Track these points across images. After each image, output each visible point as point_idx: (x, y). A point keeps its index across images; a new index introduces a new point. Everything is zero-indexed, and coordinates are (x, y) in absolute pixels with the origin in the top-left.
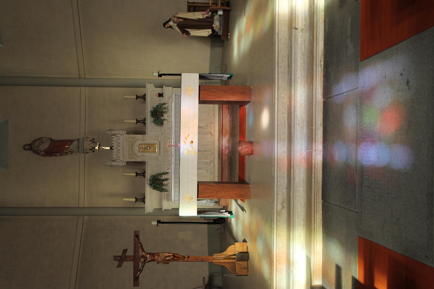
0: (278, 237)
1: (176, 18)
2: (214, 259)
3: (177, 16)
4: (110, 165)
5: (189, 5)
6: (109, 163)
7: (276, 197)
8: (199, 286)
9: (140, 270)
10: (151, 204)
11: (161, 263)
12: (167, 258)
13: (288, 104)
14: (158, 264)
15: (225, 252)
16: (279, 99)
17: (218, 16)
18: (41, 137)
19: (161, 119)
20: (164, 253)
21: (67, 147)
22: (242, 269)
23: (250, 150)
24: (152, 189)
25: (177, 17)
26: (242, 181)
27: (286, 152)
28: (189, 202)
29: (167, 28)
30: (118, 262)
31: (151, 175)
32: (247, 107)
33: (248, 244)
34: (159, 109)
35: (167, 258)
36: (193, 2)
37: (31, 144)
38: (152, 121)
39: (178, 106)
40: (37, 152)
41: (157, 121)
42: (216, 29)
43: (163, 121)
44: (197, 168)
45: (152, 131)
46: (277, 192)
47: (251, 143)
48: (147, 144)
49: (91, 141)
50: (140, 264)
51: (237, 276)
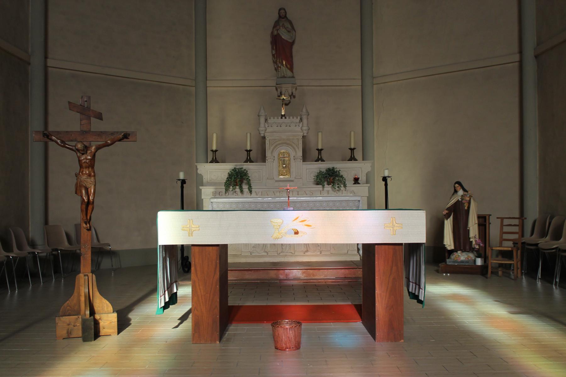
1: (468, 199)
5: (487, 217)
6: (263, 113)
9: (62, 142)
10: (208, 171)
11: (77, 179)
12: (84, 192)
14: (76, 174)
17: (474, 258)
18: (296, 30)
19: (324, 182)
20: (95, 185)
23: (284, 345)
24: (229, 171)
25: (470, 200)
29: (454, 186)
31: (248, 171)
32: (359, 325)
34: (338, 179)
36: (490, 222)
37: (287, 18)
38: (321, 170)
40: (276, 24)
42: (454, 256)
43: (321, 185)
47: (298, 347)
48: (289, 164)
49: (292, 93)
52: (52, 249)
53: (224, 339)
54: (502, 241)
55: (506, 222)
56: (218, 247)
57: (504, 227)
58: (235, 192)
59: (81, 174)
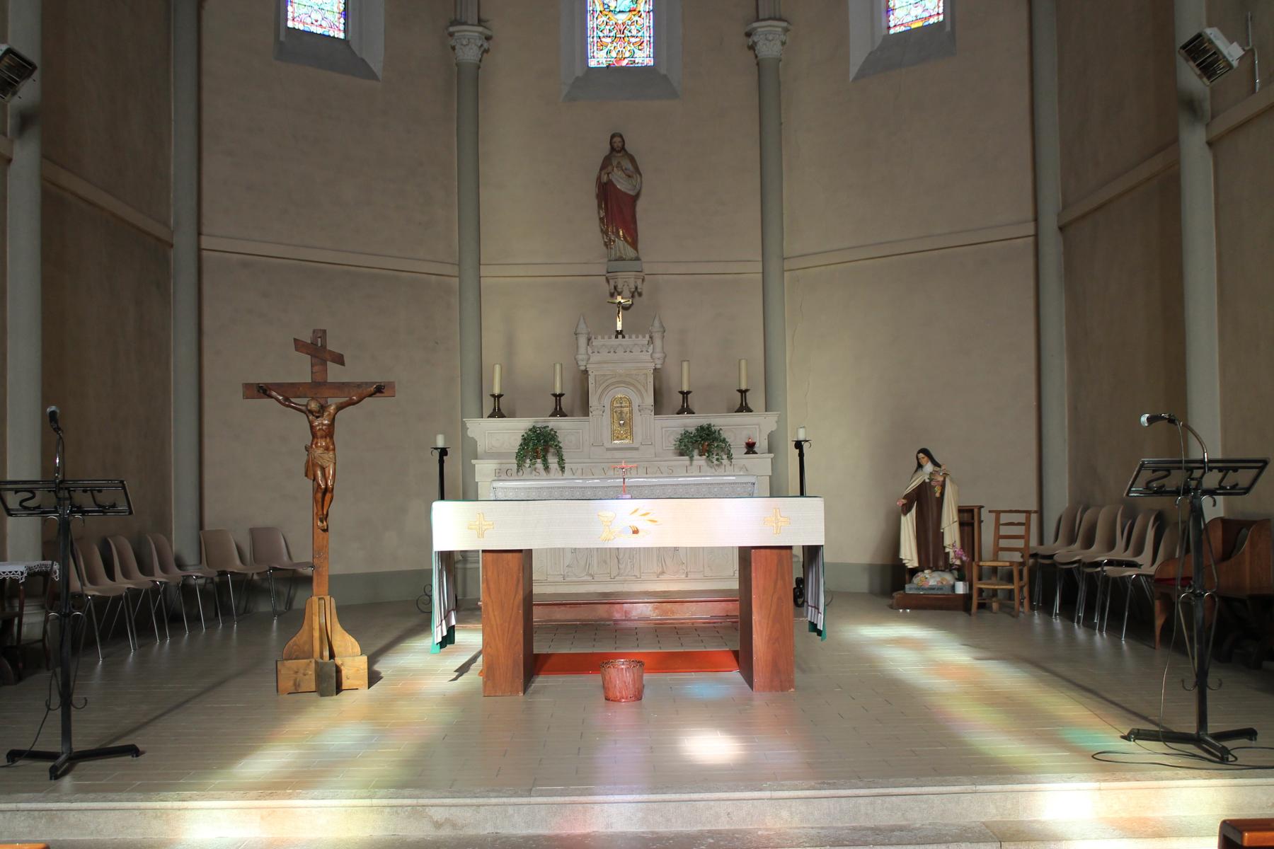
0: (346, 811)
1: (941, 479)
2: (319, 599)
5: (976, 511)
6: (582, 328)
7: (468, 801)
8: (292, 554)
9: (287, 399)
10: (487, 432)
12: (319, 473)
13: (760, 833)
14: (306, 447)
15: (341, 629)
16: (773, 801)
17: (952, 583)
18: (642, 172)
19: (692, 451)
20: (335, 464)
21: (619, 232)
22: (295, 676)
23: (618, 694)
24: (523, 432)
25: (944, 481)
26: (534, 665)
27: (610, 830)
28: (471, 529)
30: (310, 342)
32: (736, 675)
33: (364, 692)
34: (717, 446)
35: (319, 473)
37: (625, 151)
38: (687, 429)
41: (688, 442)
42: (918, 579)
44: (563, 549)
46: (483, 805)
47: (638, 696)
48: (631, 419)
49: (636, 288)
50: (303, 401)
51: (277, 662)
52: (218, 572)
53: (530, 690)
54: (998, 552)
55: (1004, 518)
56: (521, 554)
57: (1001, 527)
58: (535, 469)
59: (314, 446)
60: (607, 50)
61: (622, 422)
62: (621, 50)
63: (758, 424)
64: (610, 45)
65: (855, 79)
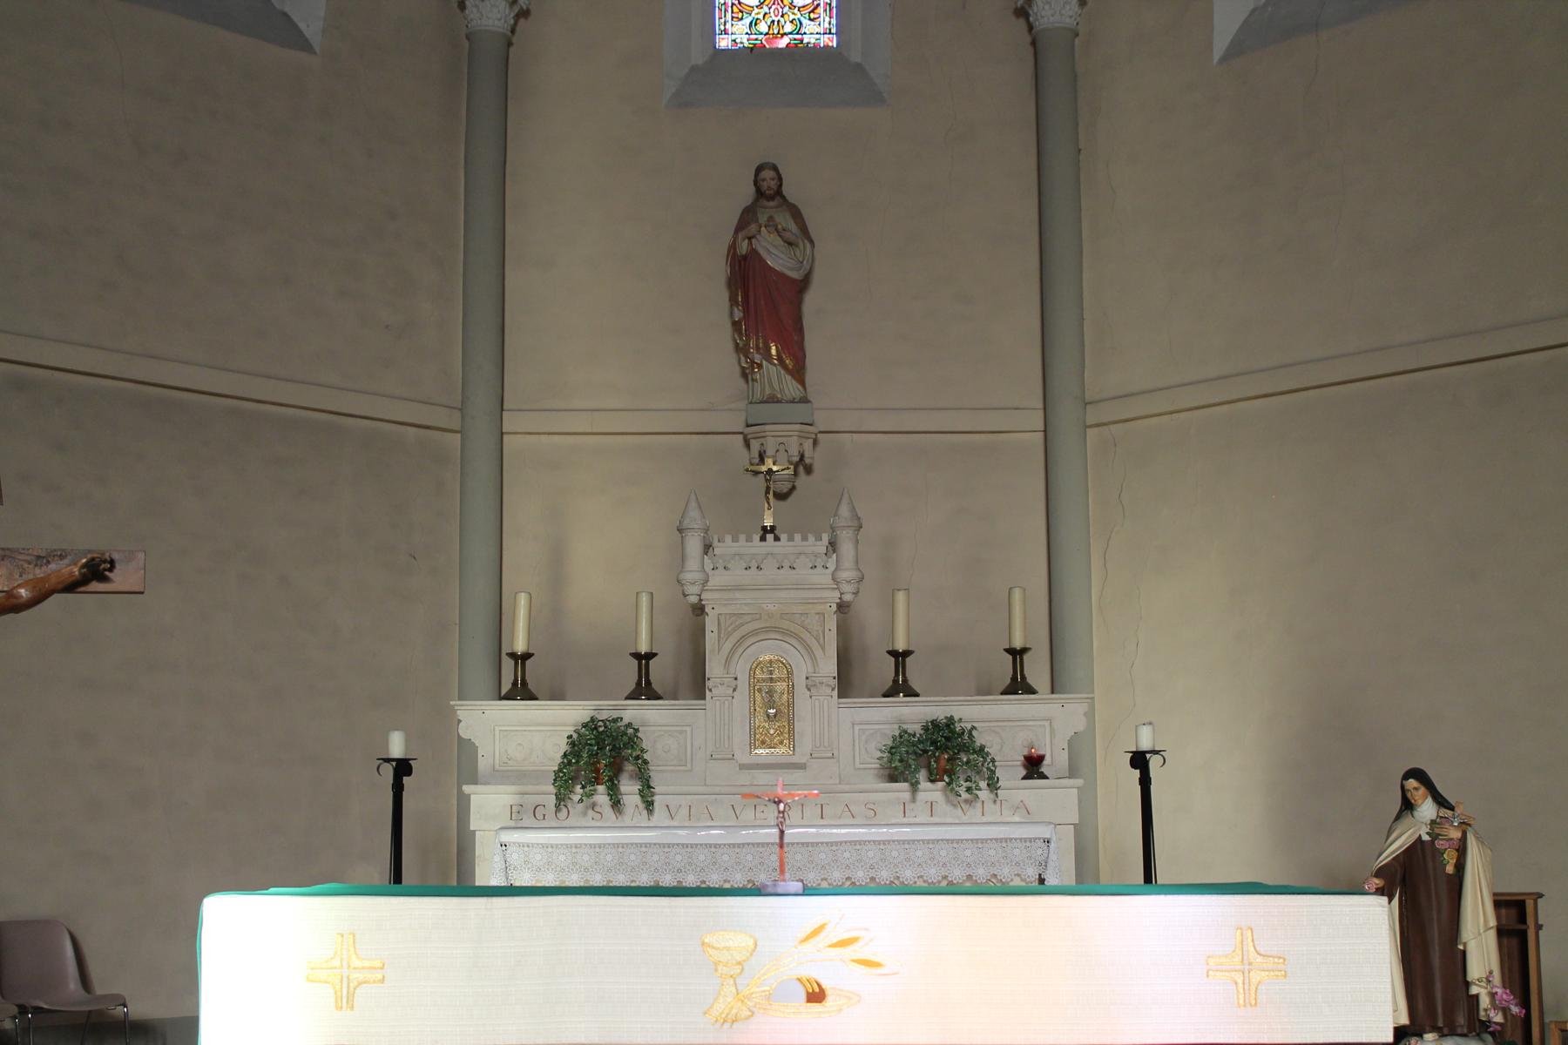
1: (1456, 834)
3: (1471, 840)
4: (686, 523)
6: (694, 519)
10: (497, 728)
19: (917, 770)
21: (770, 348)
24: (570, 730)
25: (1464, 839)
29: (1403, 787)
34: (968, 762)
37: (784, 198)
38: (905, 727)
39: (992, 852)
40: (747, 217)
41: (907, 752)
43: (905, 781)
45: (857, 728)
48: (791, 704)
49: (802, 457)
60: (750, 19)
61: (772, 711)
62: (776, 19)
63: (1050, 720)
64: (756, 10)
65: (1225, 58)
